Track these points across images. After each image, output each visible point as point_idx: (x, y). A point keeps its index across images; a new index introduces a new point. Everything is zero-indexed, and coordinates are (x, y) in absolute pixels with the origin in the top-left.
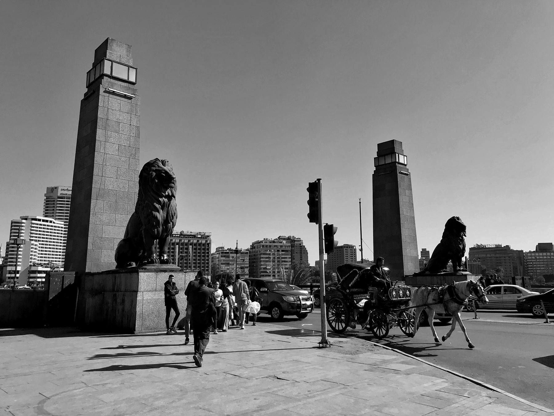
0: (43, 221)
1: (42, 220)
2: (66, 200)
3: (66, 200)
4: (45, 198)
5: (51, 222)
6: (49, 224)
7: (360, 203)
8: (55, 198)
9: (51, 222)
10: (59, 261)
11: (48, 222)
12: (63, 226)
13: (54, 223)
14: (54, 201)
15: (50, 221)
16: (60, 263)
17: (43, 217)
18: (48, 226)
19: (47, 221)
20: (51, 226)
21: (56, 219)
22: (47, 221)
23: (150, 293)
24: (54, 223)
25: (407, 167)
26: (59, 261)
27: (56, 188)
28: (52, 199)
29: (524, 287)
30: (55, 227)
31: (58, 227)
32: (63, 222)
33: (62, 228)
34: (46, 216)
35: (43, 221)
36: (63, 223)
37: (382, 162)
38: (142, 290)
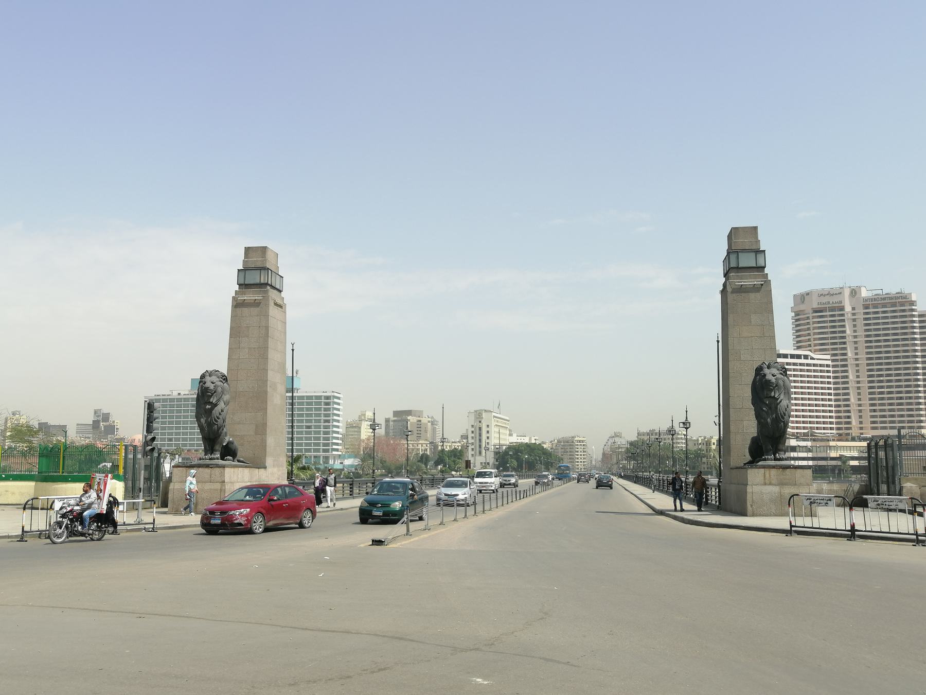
0: (793, 356)
1: (803, 357)
2: (828, 313)
3: (828, 313)
4: (793, 314)
5: (806, 357)
6: (802, 361)
7: (293, 350)
8: (809, 314)
9: (806, 357)
10: (831, 429)
11: (788, 358)
12: (829, 363)
13: (812, 359)
14: (808, 318)
15: (804, 355)
16: (834, 431)
17: (794, 349)
18: (801, 364)
19: (799, 357)
20: (808, 365)
21: (815, 351)
22: (799, 357)
23: (180, 484)
24: (812, 359)
25: (283, 294)
26: (831, 429)
27: (808, 294)
28: (804, 315)
29: (394, 478)
30: (814, 365)
31: (821, 365)
32: (829, 356)
33: (828, 366)
34: (799, 348)
35: (793, 356)
36: (828, 357)
37: (241, 298)
38: (175, 481)
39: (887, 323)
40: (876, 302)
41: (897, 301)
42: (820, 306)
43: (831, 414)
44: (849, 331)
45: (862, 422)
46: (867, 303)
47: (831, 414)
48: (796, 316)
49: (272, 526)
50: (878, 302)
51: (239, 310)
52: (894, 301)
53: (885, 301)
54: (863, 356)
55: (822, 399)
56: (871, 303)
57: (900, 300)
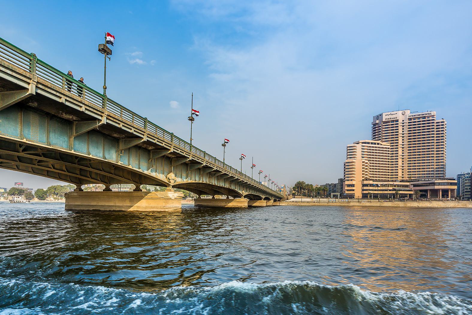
0: (372, 143)
5: (378, 144)
9: (378, 144)
12: (389, 147)
13: (381, 145)
19: (375, 144)
22: (375, 144)
27: (381, 115)
33: (389, 148)
35: (372, 143)
39: (418, 133)
40: (414, 117)
41: (426, 116)
42: (386, 120)
43: (388, 155)
44: (400, 131)
45: (404, 128)
46: (410, 117)
47: (388, 155)
48: (373, 126)
49: (136, 140)
50: (416, 117)
51: (69, 176)
52: (424, 116)
53: (420, 116)
54: (406, 143)
55: (385, 166)
56: (412, 117)
57: (428, 115)
